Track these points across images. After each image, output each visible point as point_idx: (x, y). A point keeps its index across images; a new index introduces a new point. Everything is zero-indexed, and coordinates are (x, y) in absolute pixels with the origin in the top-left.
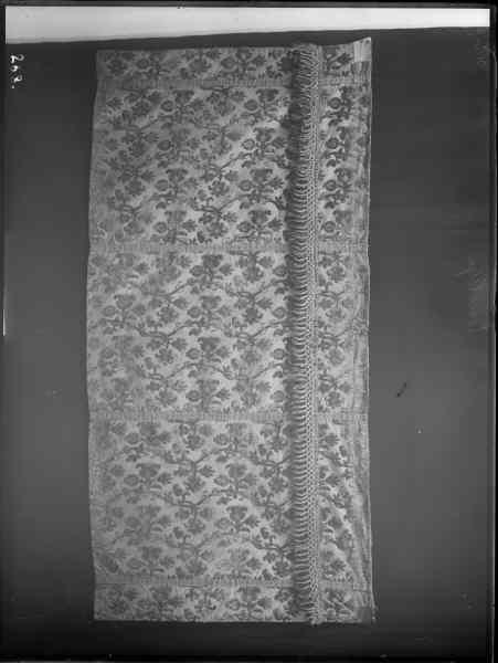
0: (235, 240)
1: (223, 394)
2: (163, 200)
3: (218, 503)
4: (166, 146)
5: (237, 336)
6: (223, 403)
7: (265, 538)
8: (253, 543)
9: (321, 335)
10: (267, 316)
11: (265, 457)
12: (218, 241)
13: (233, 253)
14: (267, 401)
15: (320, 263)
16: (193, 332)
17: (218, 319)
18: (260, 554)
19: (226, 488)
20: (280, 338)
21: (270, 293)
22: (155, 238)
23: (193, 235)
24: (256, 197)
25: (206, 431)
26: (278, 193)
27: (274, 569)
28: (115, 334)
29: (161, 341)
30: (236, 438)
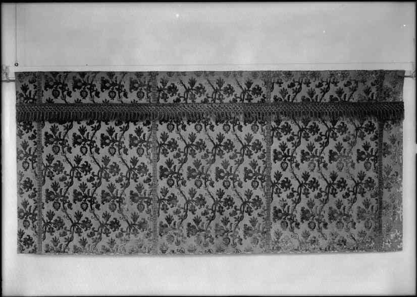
0: (149, 158)
1: (254, 165)
2: (208, 183)
3: (327, 169)
4: (85, 206)
5: (214, 156)
6: (345, 147)
7: (66, 179)
8: (125, 189)
9: (214, 100)
10: (173, 135)
11: (296, 137)
12: (150, 168)
13: (158, 159)
14: (258, 136)
15: (221, 101)
16: (212, 184)
17: (203, 169)
18: (247, 160)
19: (317, 164)
20: (188, 127)
21: (186, 134)
22: (149, 212)
23: (146, 186)
24: (64, 142)
25: (278, 176)
26: (117, 129)
27: (314, 134)
28: (213, 236)
29: (218, 205)
30: (283, 156)
